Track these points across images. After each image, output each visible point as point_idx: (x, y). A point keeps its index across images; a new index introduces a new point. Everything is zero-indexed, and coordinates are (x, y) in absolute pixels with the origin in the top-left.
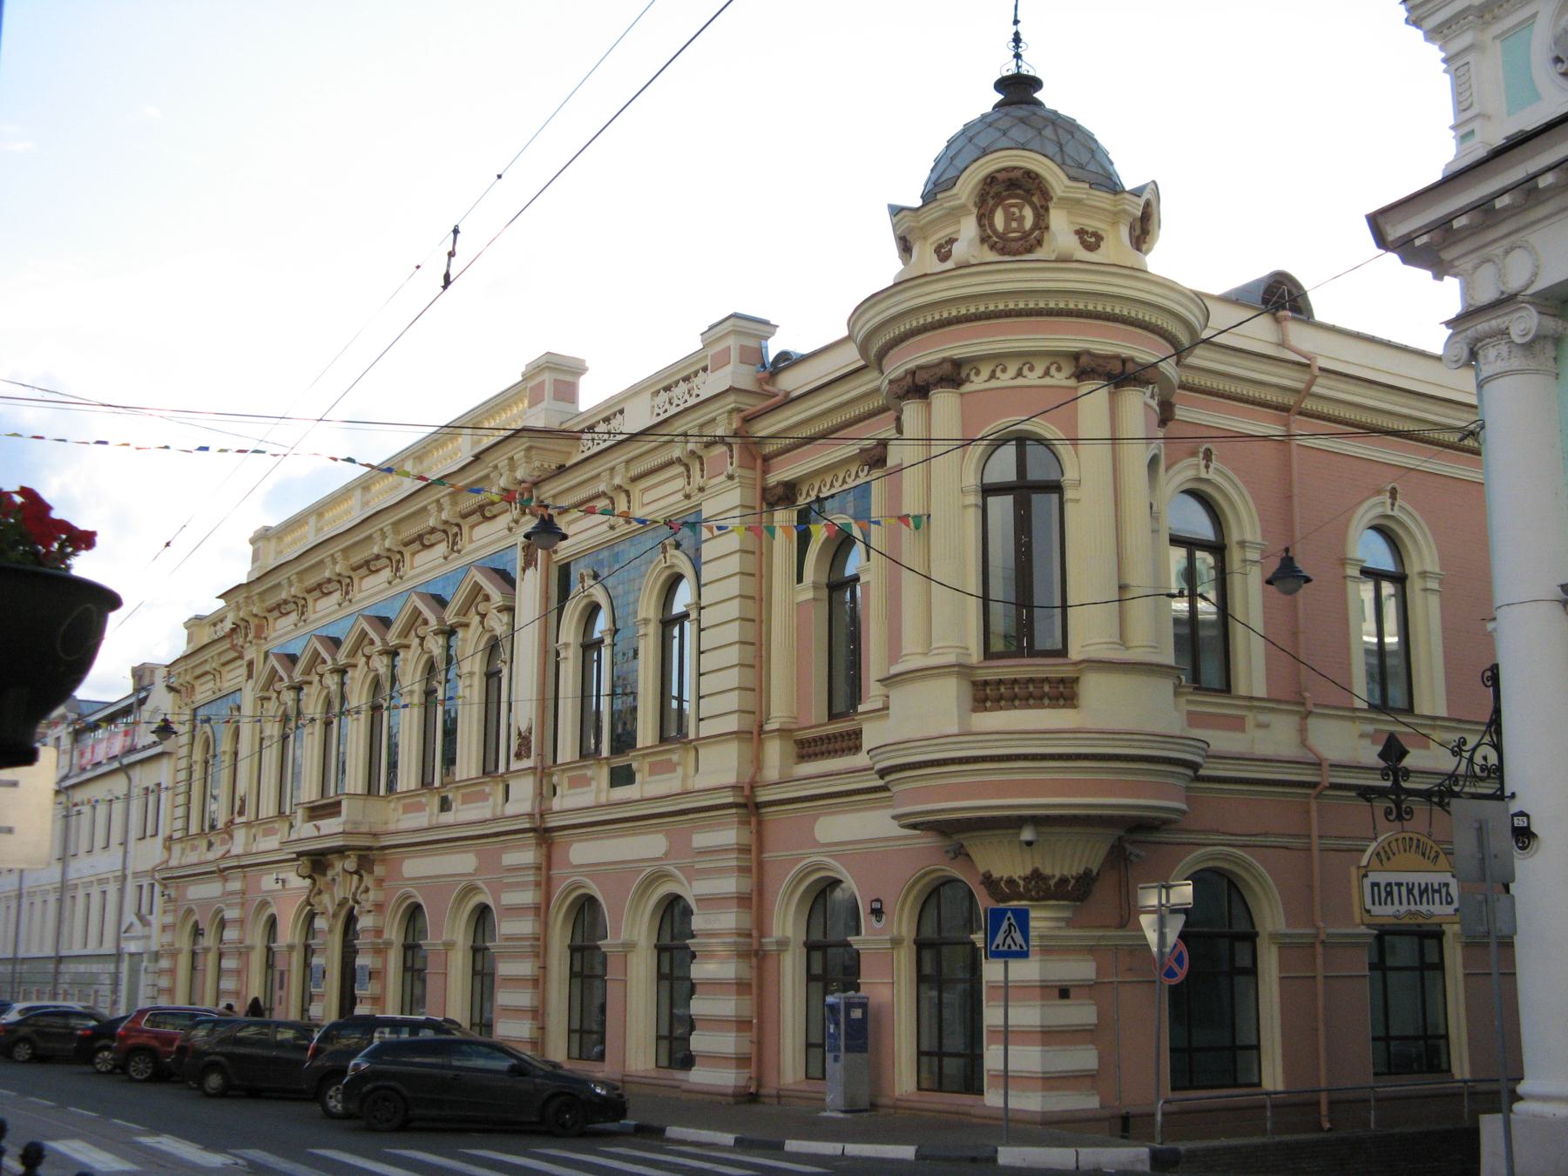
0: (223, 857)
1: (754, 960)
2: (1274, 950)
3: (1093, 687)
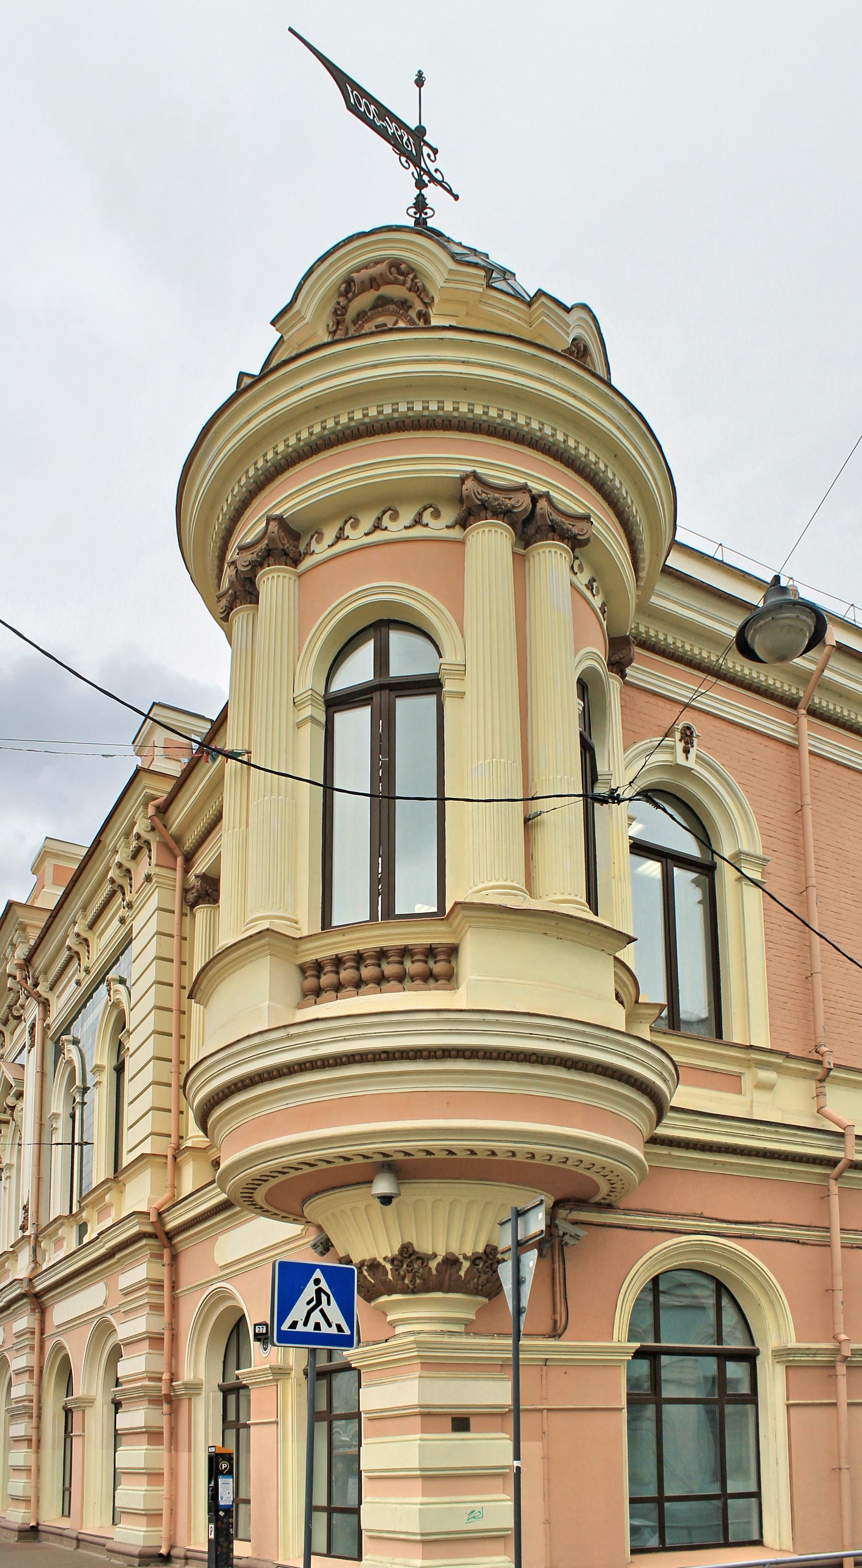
1: (166, 1407)
2: (780, 1370)
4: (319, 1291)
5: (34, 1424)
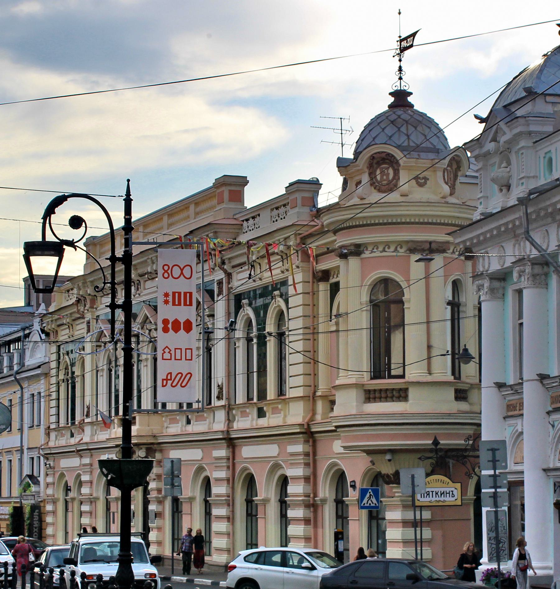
0: (79, 444)
3: (412, 393)
4: (370, 495)
5: (231, 509)
